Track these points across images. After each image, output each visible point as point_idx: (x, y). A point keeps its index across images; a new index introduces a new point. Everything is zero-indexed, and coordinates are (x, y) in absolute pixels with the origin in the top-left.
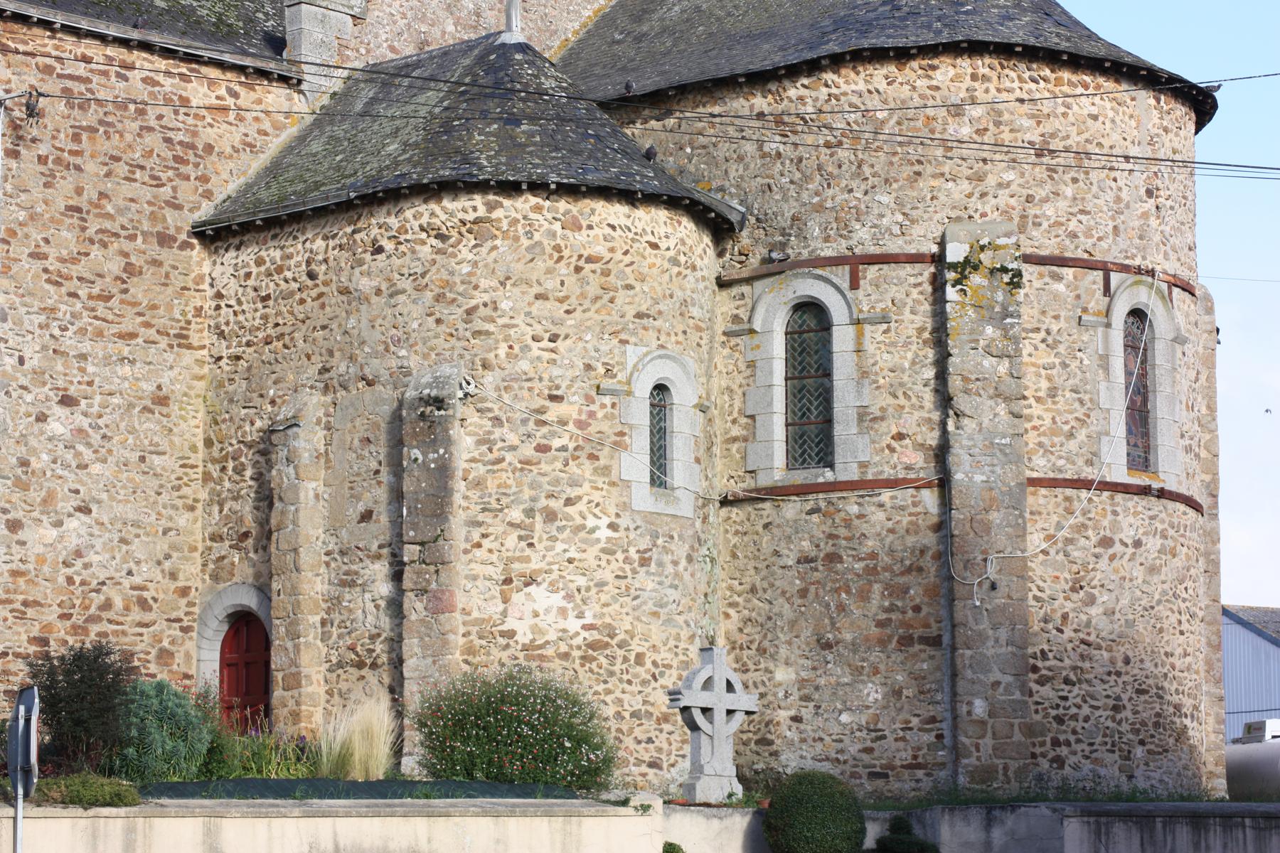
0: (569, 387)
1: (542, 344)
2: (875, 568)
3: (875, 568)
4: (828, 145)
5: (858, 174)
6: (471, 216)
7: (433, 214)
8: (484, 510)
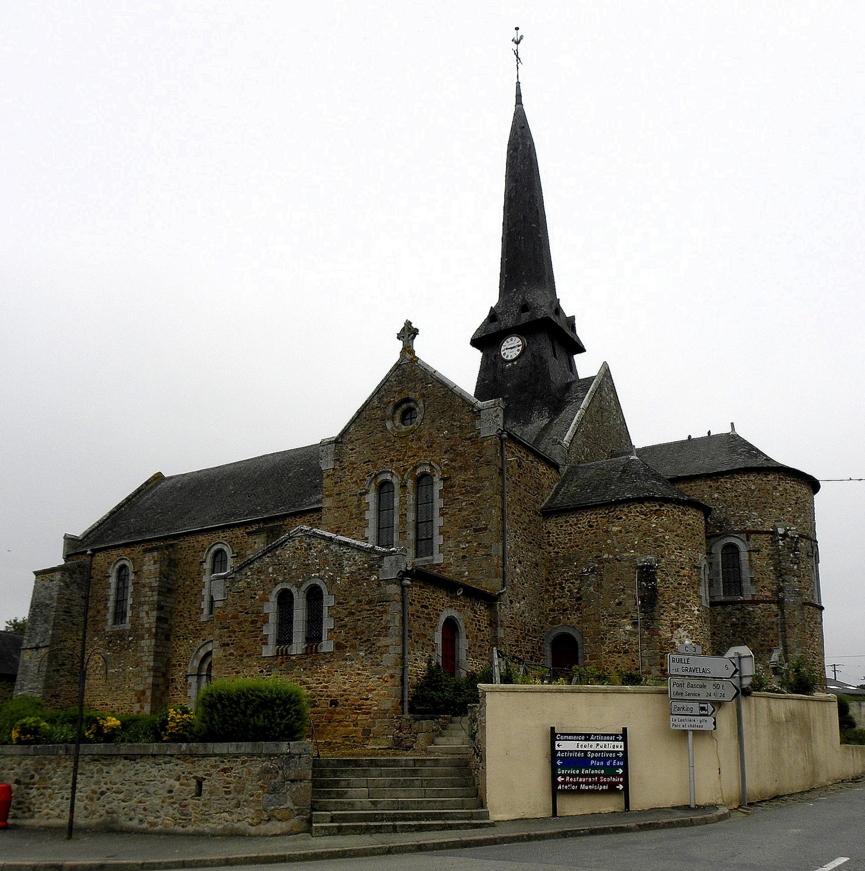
0: (686, 565)
1: (677, 551)
2: (759, 627)
3: (759, 627)
4: (736, 496)
5: (747, 506)
6: (654, 509)
7: (642, 507)
8: (664, 603)
